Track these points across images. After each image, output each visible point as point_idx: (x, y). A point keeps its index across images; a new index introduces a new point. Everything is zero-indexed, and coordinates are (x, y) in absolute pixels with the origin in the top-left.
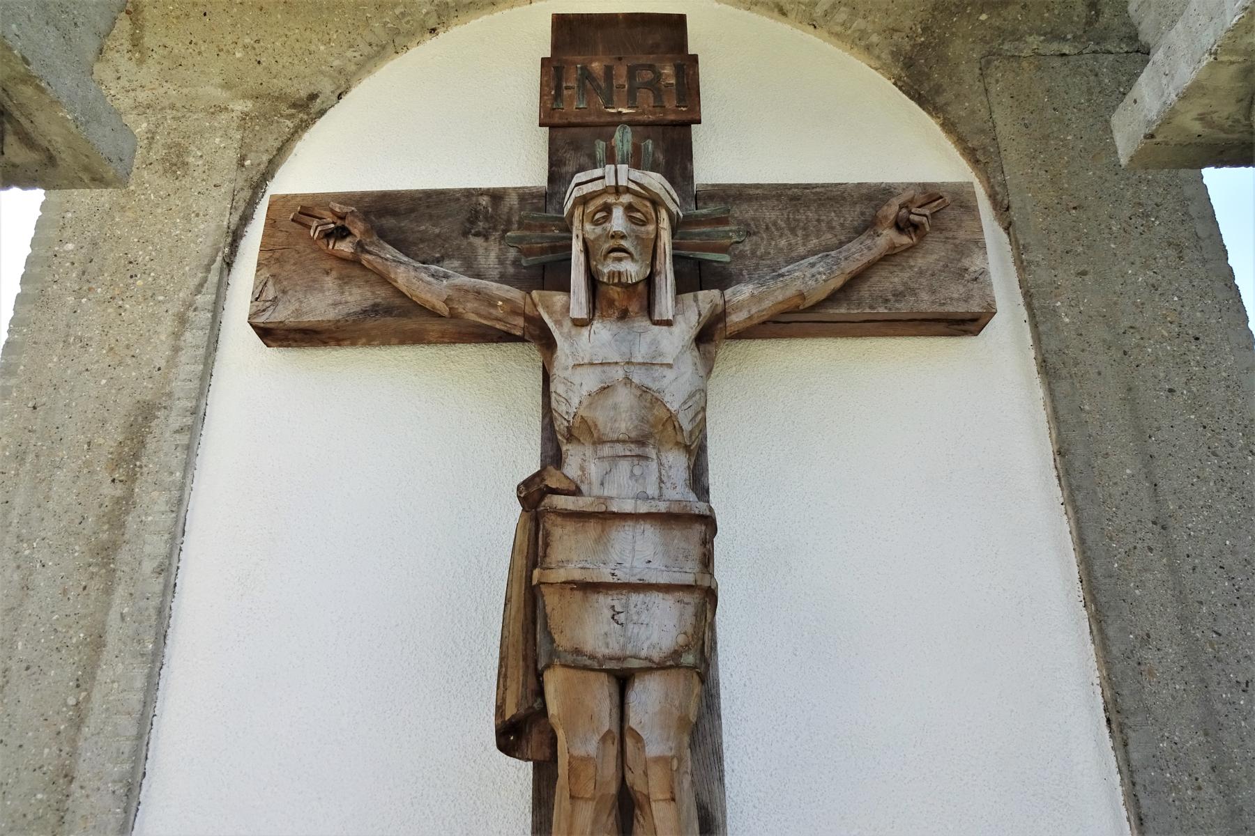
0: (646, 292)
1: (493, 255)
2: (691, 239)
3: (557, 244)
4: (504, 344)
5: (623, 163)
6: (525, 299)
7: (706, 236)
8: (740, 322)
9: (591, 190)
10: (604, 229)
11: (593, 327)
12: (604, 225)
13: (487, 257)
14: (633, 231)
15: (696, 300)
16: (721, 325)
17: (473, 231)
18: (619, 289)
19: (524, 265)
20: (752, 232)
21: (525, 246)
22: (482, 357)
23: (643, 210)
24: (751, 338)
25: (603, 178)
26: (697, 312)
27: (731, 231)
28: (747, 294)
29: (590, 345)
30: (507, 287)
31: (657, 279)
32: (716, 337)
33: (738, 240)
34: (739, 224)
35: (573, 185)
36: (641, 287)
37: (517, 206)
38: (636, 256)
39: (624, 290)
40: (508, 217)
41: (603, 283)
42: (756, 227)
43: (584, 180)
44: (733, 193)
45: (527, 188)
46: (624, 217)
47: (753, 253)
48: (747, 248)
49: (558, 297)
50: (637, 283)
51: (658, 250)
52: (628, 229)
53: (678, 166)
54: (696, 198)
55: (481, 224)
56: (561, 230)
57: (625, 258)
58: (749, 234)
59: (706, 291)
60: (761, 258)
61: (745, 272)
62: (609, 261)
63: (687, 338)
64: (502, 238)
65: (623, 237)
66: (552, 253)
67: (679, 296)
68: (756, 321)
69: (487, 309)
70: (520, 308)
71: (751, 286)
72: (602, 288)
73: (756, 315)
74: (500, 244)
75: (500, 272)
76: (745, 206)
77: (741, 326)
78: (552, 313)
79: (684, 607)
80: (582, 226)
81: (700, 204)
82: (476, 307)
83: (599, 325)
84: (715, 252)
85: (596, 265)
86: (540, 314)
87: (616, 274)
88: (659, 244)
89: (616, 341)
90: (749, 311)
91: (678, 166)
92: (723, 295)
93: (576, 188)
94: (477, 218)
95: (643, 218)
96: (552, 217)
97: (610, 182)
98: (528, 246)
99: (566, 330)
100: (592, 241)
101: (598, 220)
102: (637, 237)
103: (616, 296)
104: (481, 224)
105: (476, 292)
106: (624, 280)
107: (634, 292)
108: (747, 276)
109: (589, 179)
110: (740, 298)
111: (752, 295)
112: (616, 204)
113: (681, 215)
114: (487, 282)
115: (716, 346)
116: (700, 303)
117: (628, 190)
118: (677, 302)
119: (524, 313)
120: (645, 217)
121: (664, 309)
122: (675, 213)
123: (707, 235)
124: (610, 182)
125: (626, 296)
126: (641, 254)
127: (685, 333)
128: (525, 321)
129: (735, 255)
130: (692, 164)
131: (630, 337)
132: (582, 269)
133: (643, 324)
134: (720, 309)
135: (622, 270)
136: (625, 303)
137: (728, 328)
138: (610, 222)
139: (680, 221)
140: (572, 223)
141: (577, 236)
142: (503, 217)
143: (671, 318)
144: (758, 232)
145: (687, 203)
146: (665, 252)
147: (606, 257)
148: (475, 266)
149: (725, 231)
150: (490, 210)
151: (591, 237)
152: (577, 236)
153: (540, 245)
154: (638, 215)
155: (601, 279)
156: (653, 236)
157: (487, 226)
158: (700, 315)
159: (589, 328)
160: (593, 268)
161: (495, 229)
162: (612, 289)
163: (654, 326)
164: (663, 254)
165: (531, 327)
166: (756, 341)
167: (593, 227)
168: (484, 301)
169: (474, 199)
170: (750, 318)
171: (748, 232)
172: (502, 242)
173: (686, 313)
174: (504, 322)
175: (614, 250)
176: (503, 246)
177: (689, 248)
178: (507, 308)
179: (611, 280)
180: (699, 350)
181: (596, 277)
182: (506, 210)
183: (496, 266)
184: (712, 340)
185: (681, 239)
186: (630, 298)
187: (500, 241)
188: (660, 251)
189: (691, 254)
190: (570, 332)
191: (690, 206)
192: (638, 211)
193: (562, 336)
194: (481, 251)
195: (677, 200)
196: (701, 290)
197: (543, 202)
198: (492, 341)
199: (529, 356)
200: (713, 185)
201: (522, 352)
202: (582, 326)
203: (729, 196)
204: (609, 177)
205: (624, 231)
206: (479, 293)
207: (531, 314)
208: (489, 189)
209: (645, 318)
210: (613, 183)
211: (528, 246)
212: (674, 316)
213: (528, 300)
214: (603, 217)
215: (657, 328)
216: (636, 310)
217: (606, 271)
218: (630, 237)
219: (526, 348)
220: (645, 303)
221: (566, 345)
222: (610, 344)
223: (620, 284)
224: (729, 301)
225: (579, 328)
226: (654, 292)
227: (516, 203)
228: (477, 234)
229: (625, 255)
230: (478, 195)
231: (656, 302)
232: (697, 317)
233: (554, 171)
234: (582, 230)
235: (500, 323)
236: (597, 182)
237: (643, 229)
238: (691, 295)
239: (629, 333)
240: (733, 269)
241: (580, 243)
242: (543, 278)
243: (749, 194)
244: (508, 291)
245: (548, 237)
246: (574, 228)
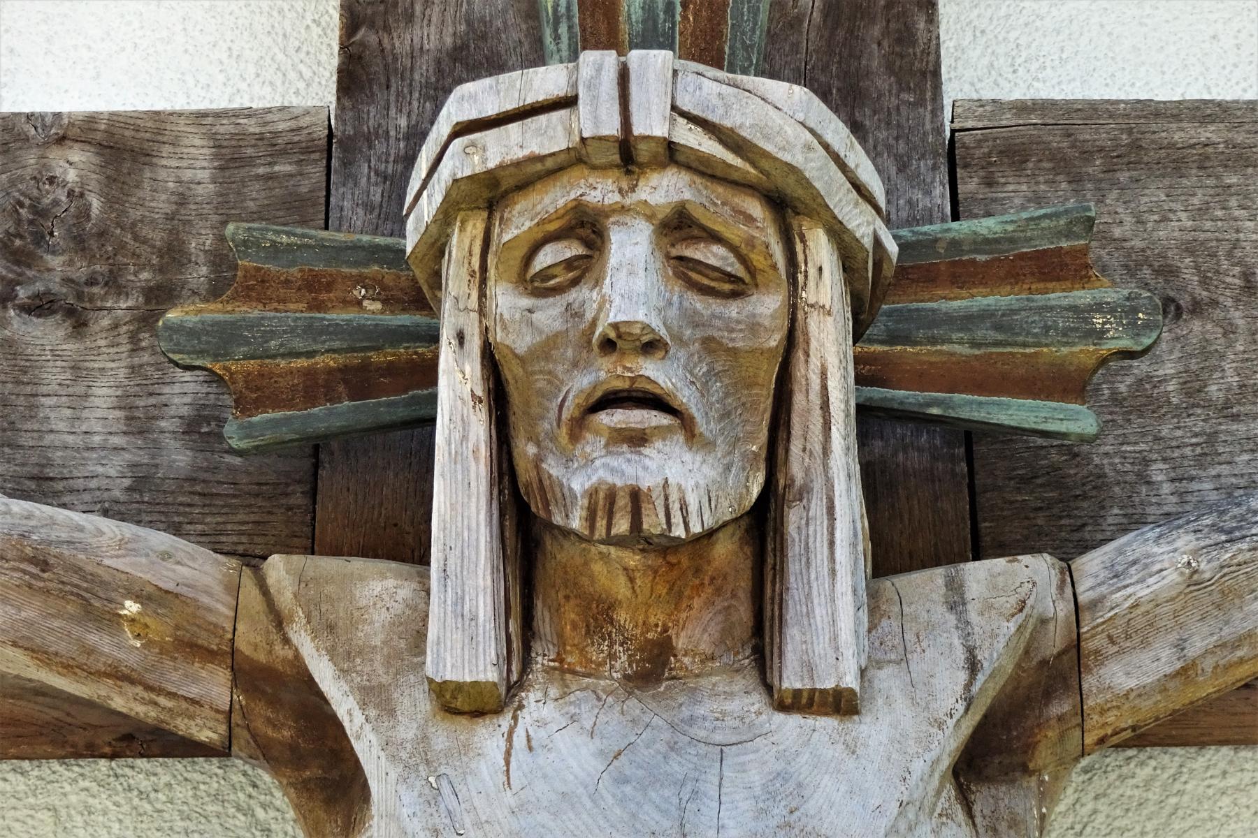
0: (745, 565)
1: (103, 394)
2: (933, 341)
3: (375, 357)
4: (141, 763)
5: (651, 38)
6: (235, 590)
7: (998, 327)
8: (1142, 692)
9: (520, 154)
10: (574, 313)
11: (526, 718)
12: (573, 295)
13: (79, 401)
14: (694, 320)
15: (956, 600)
16: (1061, 707)
17: (22, 293)
18: (633, 559)
19: (235, 443)
20: (1185, 301)
21: (239, 365)
22: (45, 816)
23: (736, 232)
24: (1184, 743)
25: (569, 102)
26: (960, 655)
27: (1099, 307)
28: (1172, 577)
29: (509, 798)
30: (160, 539)
31: (793, 517)
32: (1043, 756)
33: (1126, 343)
34: (1131, 271)
35: (442, 128)
36: (725, 549)
37: (206, 190)
38: (702, 425)
39: (654, 560)
40: (173, 232)
41: (567, 533)
42: (1205, 282)
43: (491, 110)
44: (1103, 139)
45: (249, 113)
46: (657, 263)
47: (1193, 389)
48: (1169, 369)
49: (377, 587)
50: (710, 534)
51: (799, 400)
52: (673, 313)
53: (876, 31)
54: (952, 157)
55: (56, 262)
56: (389, 302)
57: (669, 429)
58: (1172, 309)
59: (1001, 562)
60: (1226, 410)
61: (1158, 472)
62: (593, 445)
63: (918, 767)
64: (146, 320)
65: (651, 346)
66: (352, 399)
67: (886, 584)
68: (1206, 688)
69: (77, 631)
70: (214, 629)
71: (1185, 541)
72: (560, 555)
73: (1209, 663)
74: (136, 349)
75: (133, 466)
76: (1154, 194)
77: (1148, 708)
78: (348, 656)
79: (966, 166)
80: (482, 295)
81: (969, 185)
82: (29, 624)
83: (548, 711)
84: (1035, 395)
85: (538, 461)
86: (297, 656)
87: (623, 501)
88: (799, 371)
89: (623, 780)
90: (1180, 646)
91: (876, 31)
92: (1068, 576)
93: (458, 143)
94: (39, 239)
95: (737, 269)
96: (355, 247)
97: (596, 120)
98: (253, 365)
99: (407, 730)
100: (522, 360)
101: (545, 274)
102: (710, 345)
103: (621, 589)
104: (56, 262)
105: (33, 560)
106: (653, 523)
107: (698, 571)
108: (1167, 488)
109: (510, 105)
110: (1142, 592)
111: (1193, 580)
112: (624, 209)
113: (892, 248)
114: (77, 517)
115: (1046, 796)
116: (973, 617)
117: (671, 154)
118: (874, 606)
119: (233, 652)
120: (743, 260)
121: (821, 646)
122: (868, 242)
123: (1000, 322)
124: (596, 120)
125: (662, 590)
126: (725, 415)
127: (913, 748)
128: (235, 682)
129: (1116, 399)
130: (932, 19)
131: (676, 767)
132: (480, 471)
133: (734, 706)
134: (1054, 641)
135: (646, 482)
136: (658, 616)
137: (1094, 720)
138: (598, 283)
139: (888, 271)
140: (436, 279)
141: (461, 337)
142: (146, 231)
143: (851, 681)
144: (1215, 303)
145: (916, 180)
146: (825, 406)
147: (578, 426)
148: (27, 440)
149: (1074, 308)
150: (96, 204)
151: (515, 340)
152: (461, 337)
153: (302, 363)
154: (714, 255)
155: (558, 519)
156: (774, 340)
157: (81, 270)
158: (973, 666)
159: (505, 721)
160: (525, 472)
161: (115, 284)
162: (604, 557)
163: (780, 717)
164: (817, 413)
165: (261, 710)
166: (1210, 752)
167: (526, 302)
168: (62, 596)
169: (30, 159)
170: (1185, 673)
171: (1168, 301)
172: (146, 340)
173: (914, 658)
174: (149, 688)
175: (611, 400)
176: (146, 357)
177: (922, 378)
178: (161, 629)
179: (601, 524)
180: (970, 814)
181: (536, 507)
182: (162, 204)
183: (117, 440)
184: (1026, 770)
185: (892, 339)
186: (677, 597)
187: (134, 338)
188: (803, 402)
189: (934, 401)
190: (425, 738)
191: (928, 193)
192: (715, 238)
193: (393, 758)
194: (54, 376)
195: (877, 188)
196: (977, 557)
197: (316, 172)
198: (91, 752)
199: (248, 812)
200: (1022, 108)
201: (217, 797)
202: (478, 713)
203: (1087, 155)
204: (595, 98)
205: (656, 323)
206: (45, 566)
207: (262, 657)
208: (91, 120)
209: (740, 683)
210: (612, 128)
211: (253, 365)
212: (863, 672)
213: (250, 590)
214: (569, 264)
215: (793, 722)
216: (705, 647)
217: (579, 484)
218: (681, 342)
219: (237, 778)
220: (743, 613)
221: (408, 797)
222: (594, 796)
223: (637, 538)
224: (1095, 604)
225: (463, 720)
226: (780, 572)
227: (204, 175)
228: (41, 307)
229: (664, 420)
230: (46, 145)
231: (790, 616)
232: (963, 676)
233: (362, 44)
234: (482, 312)
235: (131, 690)
236: (542, 119)
237: (733, 310)
238: (937, 576)
239: (673, 747)
240: (1107, 457)
241: (473, 368)
242: (313, 493)
243: (1172, 145)
244: (166, 556)
245: (335, 330)
246: (447, 305)
